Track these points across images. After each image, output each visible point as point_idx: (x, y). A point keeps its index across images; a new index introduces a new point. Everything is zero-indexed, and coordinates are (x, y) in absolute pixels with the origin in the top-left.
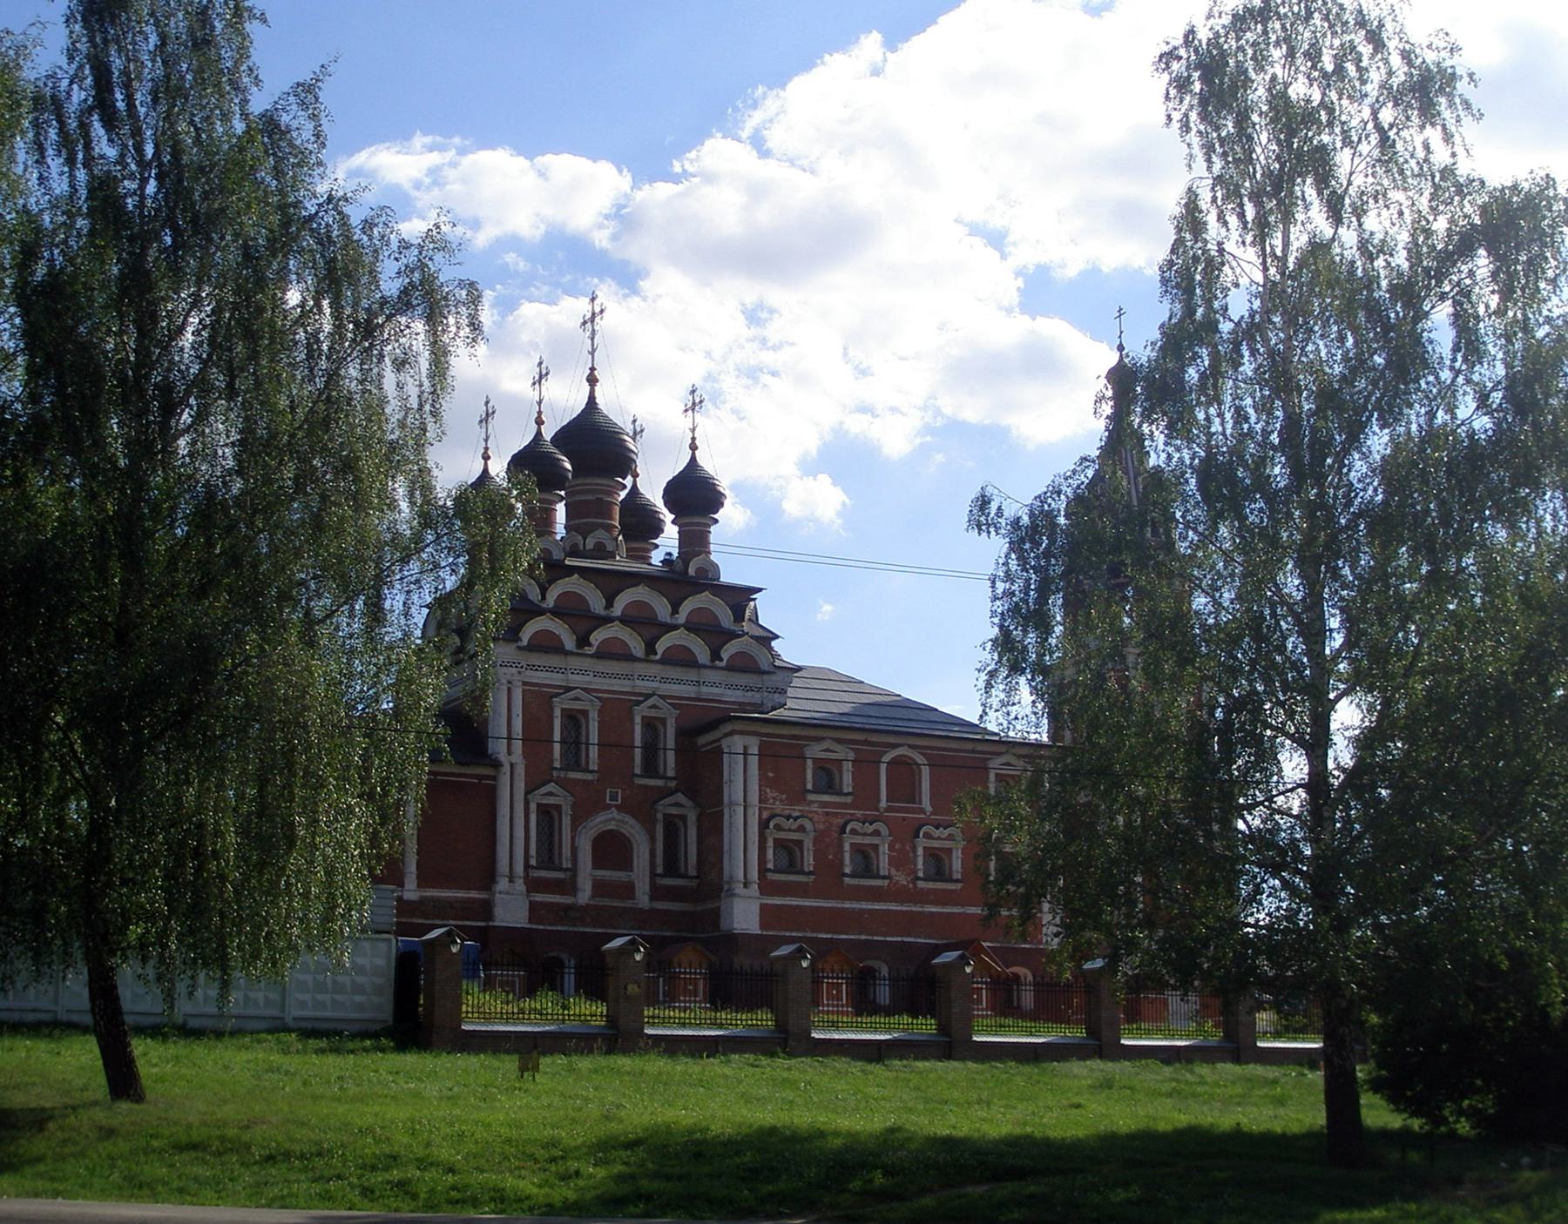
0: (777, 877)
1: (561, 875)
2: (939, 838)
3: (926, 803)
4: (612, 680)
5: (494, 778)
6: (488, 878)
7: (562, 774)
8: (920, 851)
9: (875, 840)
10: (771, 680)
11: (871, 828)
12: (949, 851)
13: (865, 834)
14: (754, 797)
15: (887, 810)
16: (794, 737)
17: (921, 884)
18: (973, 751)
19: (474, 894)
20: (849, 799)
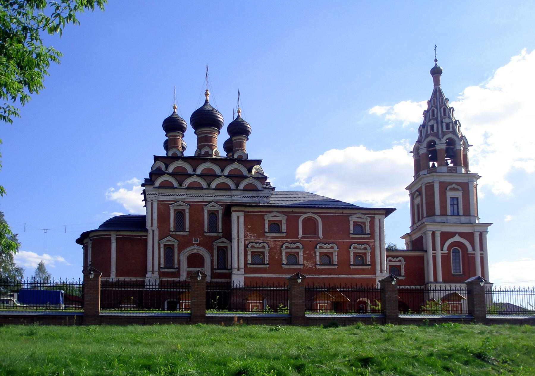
0: (252, 266)
1: (173, 270)
2: (326, 248)
3: (321, 235)
4: (195, 197)
5: (147, 236)
6: (144, 273)
7: (174, 233)
8: (318, 254)
9: (297, 250)
10: (262, 194)
11: (295, 246)
12: (332, 253)
13: (292, 248)
14: (242, 236)
15: (302, 238)
16: (260, 212)
17: (318, 267)
18: (342, 213)
19: (139, 279)
20: (285, 235)
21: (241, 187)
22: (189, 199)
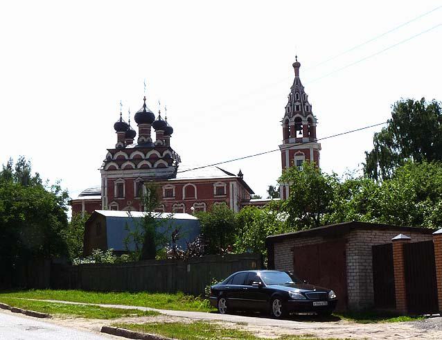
3: (196, 198)
4: (129, 174)
21: (156, 166)
22: (126, 176)
